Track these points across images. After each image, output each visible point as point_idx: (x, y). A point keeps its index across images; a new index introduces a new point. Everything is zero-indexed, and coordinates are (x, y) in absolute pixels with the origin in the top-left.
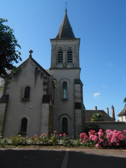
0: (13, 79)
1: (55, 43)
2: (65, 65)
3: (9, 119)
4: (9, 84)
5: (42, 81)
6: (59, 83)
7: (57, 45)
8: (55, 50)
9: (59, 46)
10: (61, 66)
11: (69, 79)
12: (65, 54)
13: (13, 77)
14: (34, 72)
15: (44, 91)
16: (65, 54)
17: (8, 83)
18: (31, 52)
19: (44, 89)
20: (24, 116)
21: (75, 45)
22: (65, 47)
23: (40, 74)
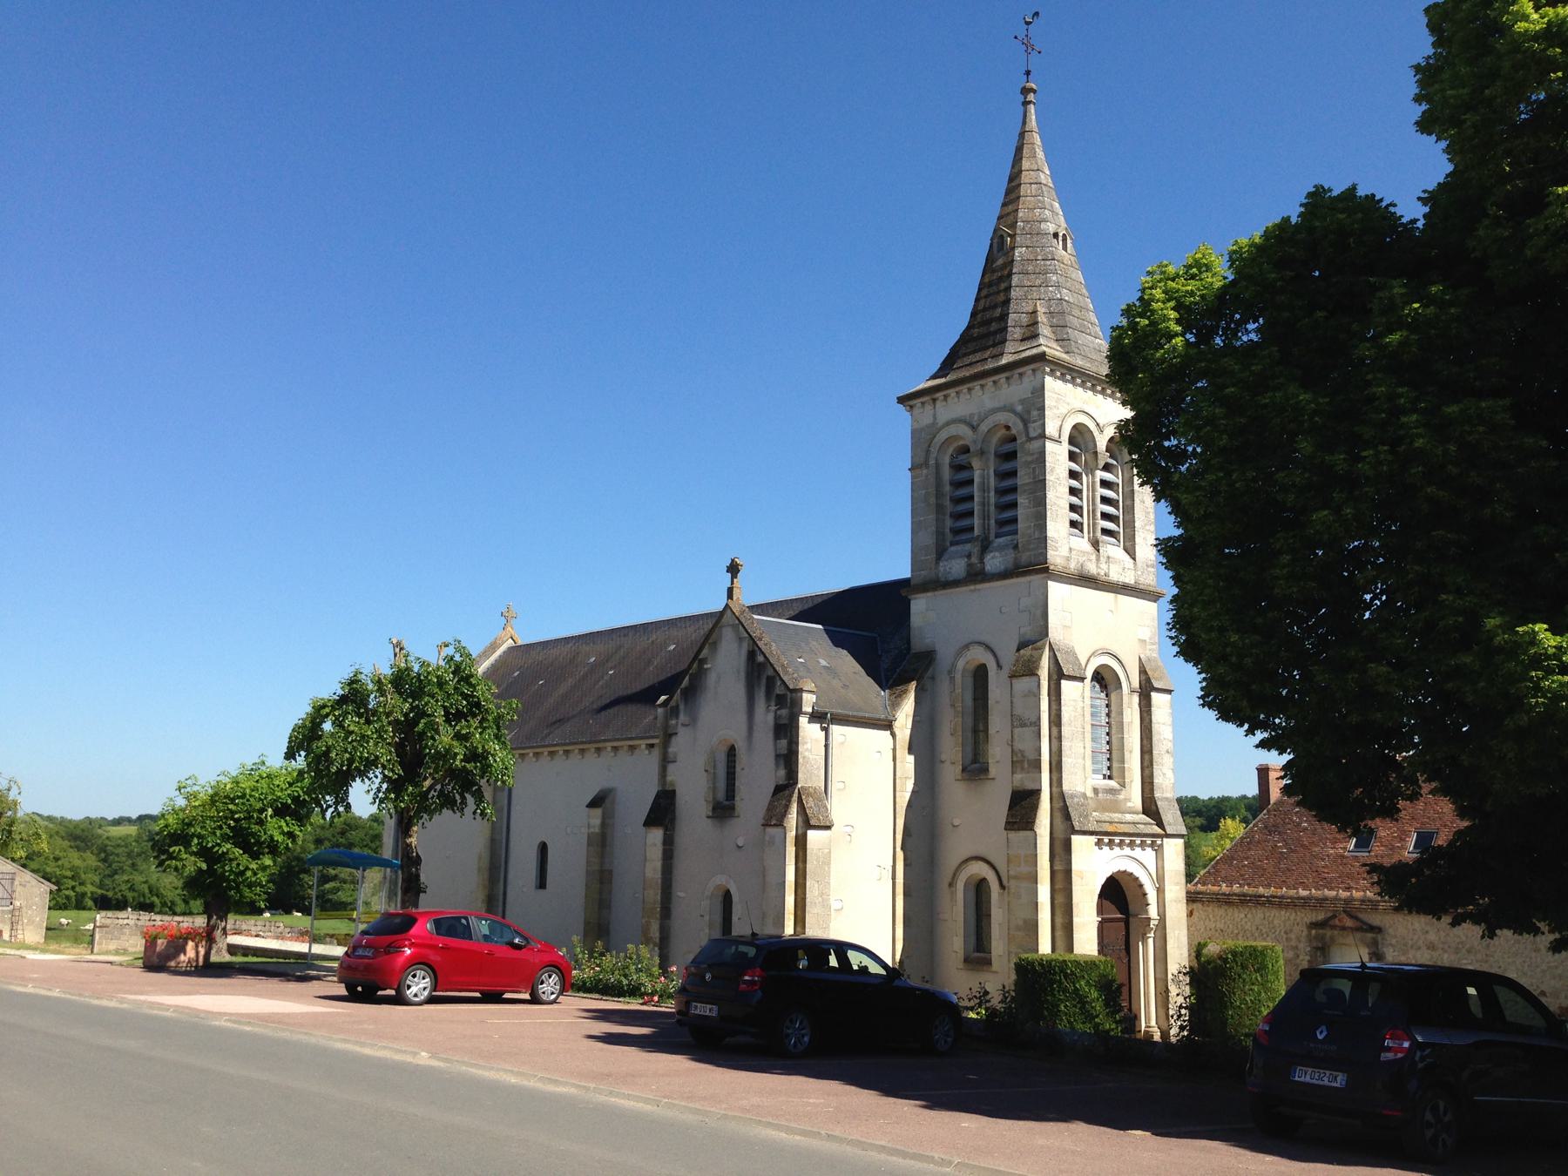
0: (683, 718)
1: (926, 415)
2: (974, 560)
3: (679, 893)
4: (674, 739)
5: (771, 718)
6: (950, 672)
7: (933, 429)
8: (926, 464)
9: (943, 435)
10: (956, 567)
11: (999, 654)
12: (983, 472)
13: (682, 707)
14: (743, 675)
15: (777, 765)
16: (983, 472)
17: (671, 735)
18: (734, 569)
19: (778, 756)
20: (720, 880)
21: (1022, 402)
22: (974, 428)
23: (764, 681)
